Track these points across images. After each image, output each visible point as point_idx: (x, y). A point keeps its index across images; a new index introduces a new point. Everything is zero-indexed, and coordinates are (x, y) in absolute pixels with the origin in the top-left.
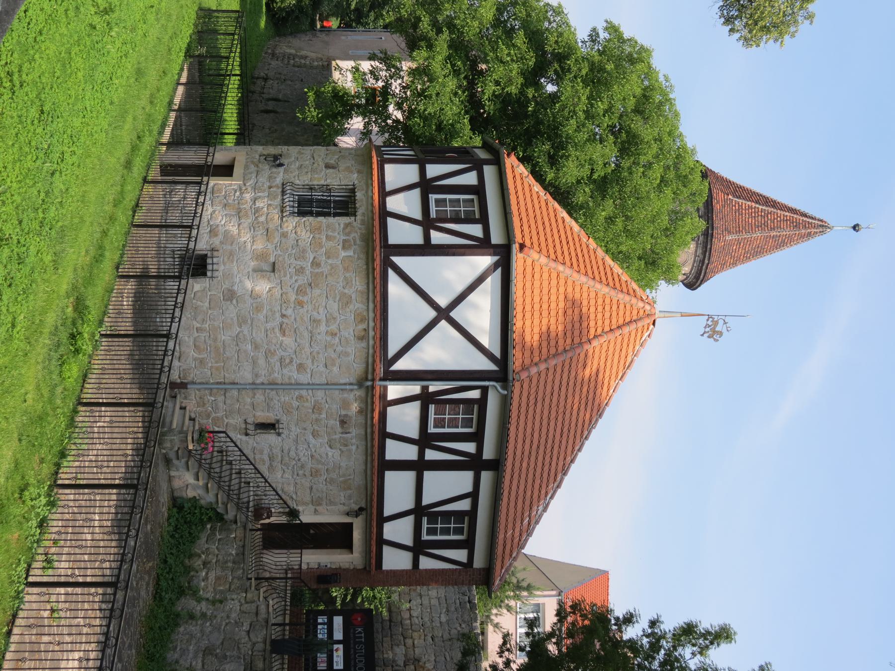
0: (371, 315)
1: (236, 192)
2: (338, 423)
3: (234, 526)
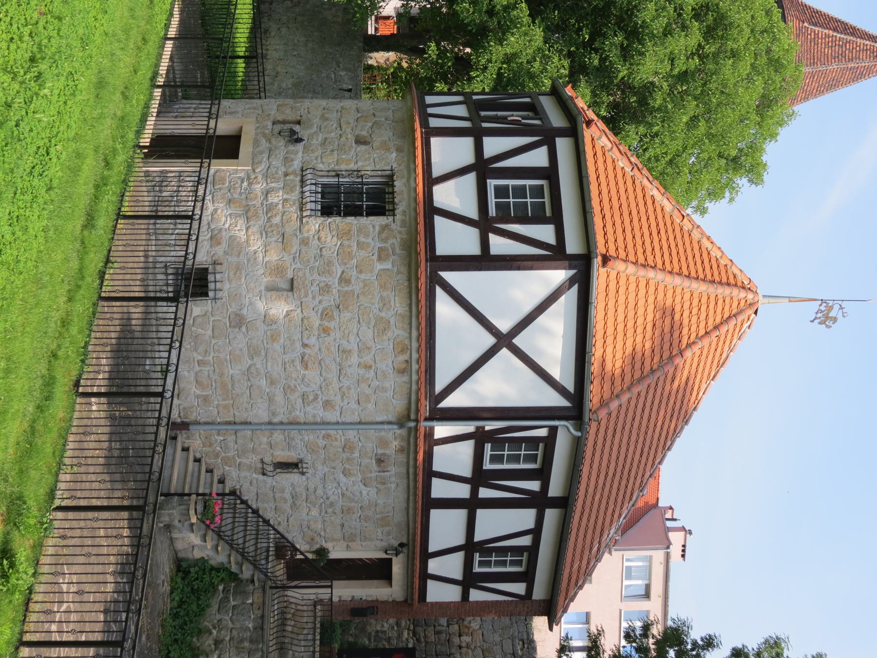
0: (415, 345)
1: (242, 182)
2: (374, 462)
3: (251, 587)
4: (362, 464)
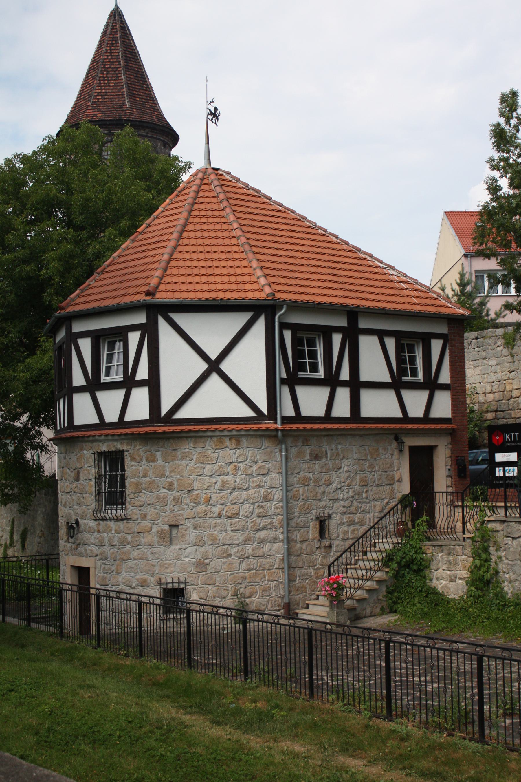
4: (320, 470)
